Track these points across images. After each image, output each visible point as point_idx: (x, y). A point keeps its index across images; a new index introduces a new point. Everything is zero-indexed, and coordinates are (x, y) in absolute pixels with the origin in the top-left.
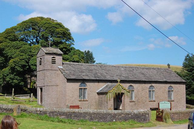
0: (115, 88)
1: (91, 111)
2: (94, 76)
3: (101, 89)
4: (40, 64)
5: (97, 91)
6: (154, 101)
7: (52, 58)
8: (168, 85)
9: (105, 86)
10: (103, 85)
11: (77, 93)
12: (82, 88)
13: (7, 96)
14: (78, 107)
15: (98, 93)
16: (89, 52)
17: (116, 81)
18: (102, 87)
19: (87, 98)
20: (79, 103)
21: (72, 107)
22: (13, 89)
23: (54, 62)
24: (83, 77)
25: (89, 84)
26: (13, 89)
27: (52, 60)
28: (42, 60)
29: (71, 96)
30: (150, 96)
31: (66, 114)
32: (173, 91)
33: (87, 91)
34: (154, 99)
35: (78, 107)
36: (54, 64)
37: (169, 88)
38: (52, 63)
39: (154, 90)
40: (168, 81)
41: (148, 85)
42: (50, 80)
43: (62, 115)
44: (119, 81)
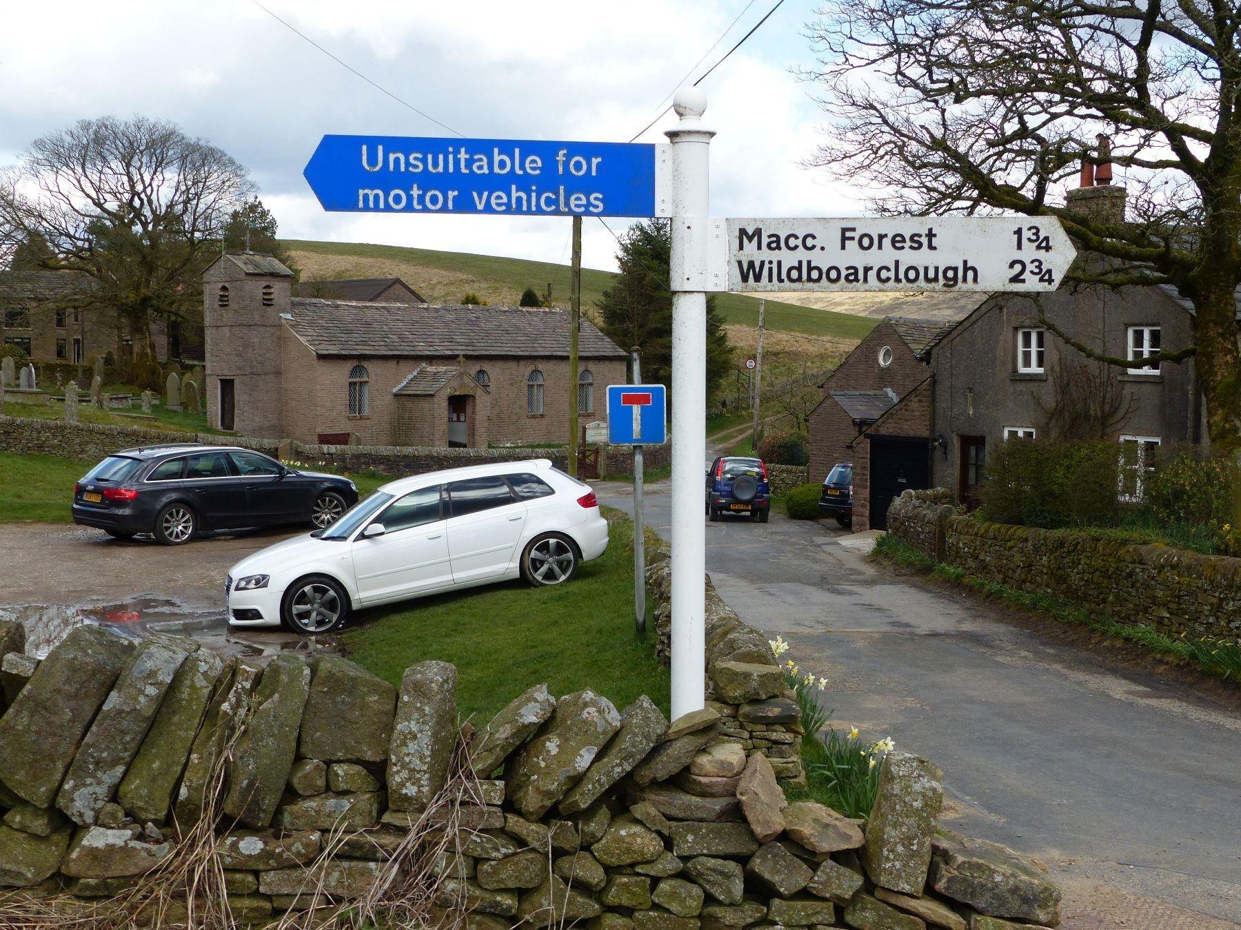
0: (447, 380)
5: (395, 390)
6: (542, 416)
8: (349, 366)
9: (415, 373)
10: (411, 372)
11: (344, 397)
13: (219, 613)
15: (396, 395)
18: (405, 378)
19: (366, 412)
21: (324, 439)
22: (562, 188)
26: (562, 188)
28: (231, 294)
29: (328, 404)
30: (530, 403)
32: (591, 384)
33: (366, 390)
34: (541, 411)
35: (342, 439)
36: (269, 309)
37: (531, 377)
39: (541, 382)
41: (526, 369)
44: (462, 359)
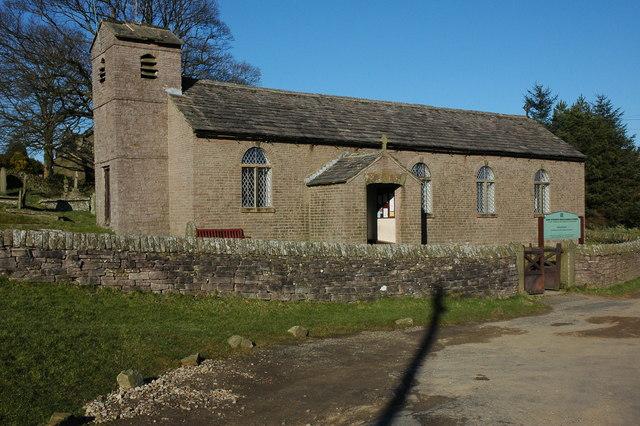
1: (280, 246)
2: (295, 126)
3: (321, 172)
4: (102, 81)
5: (307, 180)
6: (493, 216)
7: (142, 57)
9: (335, 162)
10: (329, 160)
11: (234, 185)
12: (252, 165)
14: (237, 233)
16: (603, 108)
17: (391, 146)
18: (326, 159)
20: (240, 219)
23: (148, 70)
24: (258, 127)
25: (273, 152)
27: (143, 64)
31: (160, 259)
35: (237, 233)
38: (143, 76)
40: (535, 152)
41: (475, 163)
42: (136, 139)
43: (145, 266)
